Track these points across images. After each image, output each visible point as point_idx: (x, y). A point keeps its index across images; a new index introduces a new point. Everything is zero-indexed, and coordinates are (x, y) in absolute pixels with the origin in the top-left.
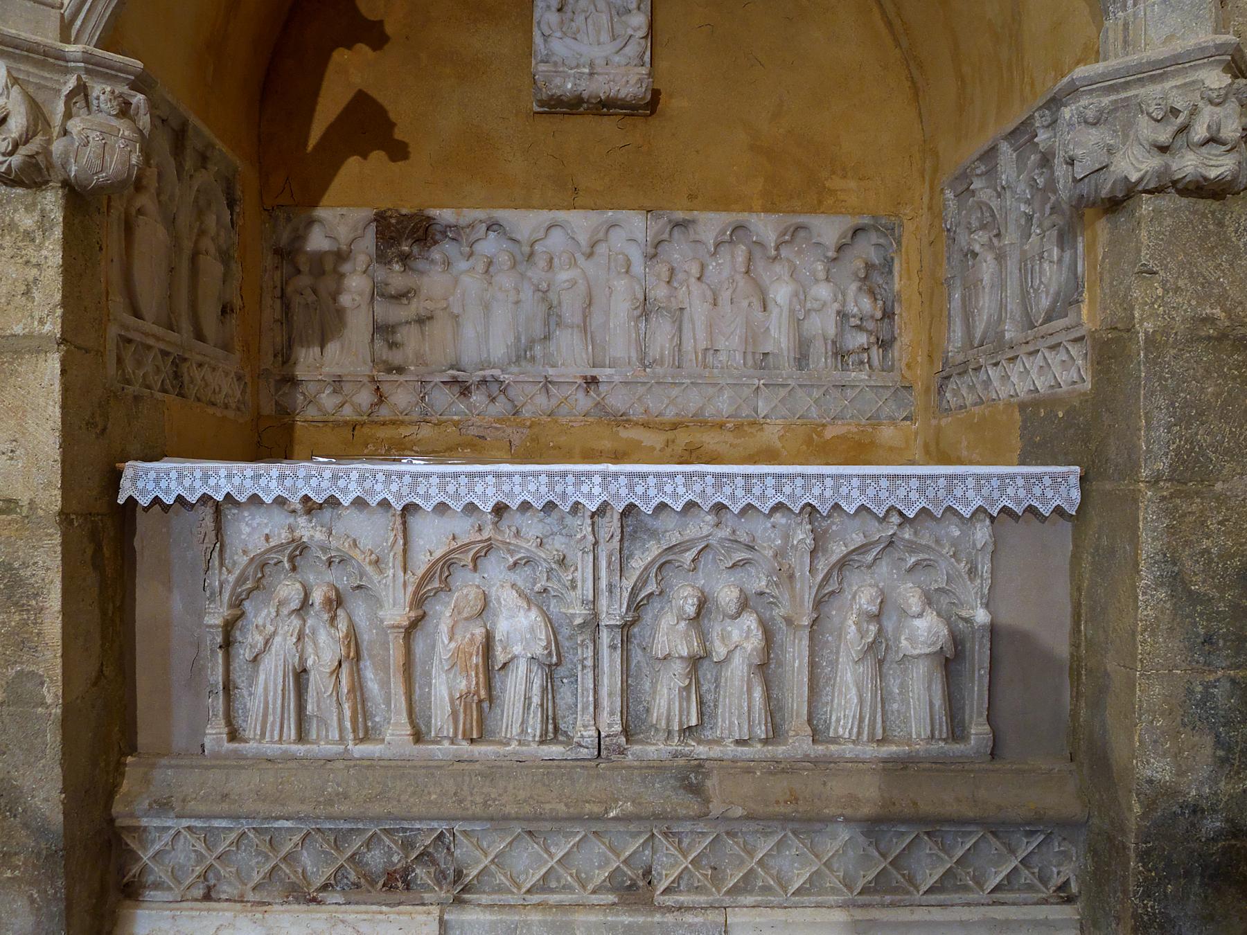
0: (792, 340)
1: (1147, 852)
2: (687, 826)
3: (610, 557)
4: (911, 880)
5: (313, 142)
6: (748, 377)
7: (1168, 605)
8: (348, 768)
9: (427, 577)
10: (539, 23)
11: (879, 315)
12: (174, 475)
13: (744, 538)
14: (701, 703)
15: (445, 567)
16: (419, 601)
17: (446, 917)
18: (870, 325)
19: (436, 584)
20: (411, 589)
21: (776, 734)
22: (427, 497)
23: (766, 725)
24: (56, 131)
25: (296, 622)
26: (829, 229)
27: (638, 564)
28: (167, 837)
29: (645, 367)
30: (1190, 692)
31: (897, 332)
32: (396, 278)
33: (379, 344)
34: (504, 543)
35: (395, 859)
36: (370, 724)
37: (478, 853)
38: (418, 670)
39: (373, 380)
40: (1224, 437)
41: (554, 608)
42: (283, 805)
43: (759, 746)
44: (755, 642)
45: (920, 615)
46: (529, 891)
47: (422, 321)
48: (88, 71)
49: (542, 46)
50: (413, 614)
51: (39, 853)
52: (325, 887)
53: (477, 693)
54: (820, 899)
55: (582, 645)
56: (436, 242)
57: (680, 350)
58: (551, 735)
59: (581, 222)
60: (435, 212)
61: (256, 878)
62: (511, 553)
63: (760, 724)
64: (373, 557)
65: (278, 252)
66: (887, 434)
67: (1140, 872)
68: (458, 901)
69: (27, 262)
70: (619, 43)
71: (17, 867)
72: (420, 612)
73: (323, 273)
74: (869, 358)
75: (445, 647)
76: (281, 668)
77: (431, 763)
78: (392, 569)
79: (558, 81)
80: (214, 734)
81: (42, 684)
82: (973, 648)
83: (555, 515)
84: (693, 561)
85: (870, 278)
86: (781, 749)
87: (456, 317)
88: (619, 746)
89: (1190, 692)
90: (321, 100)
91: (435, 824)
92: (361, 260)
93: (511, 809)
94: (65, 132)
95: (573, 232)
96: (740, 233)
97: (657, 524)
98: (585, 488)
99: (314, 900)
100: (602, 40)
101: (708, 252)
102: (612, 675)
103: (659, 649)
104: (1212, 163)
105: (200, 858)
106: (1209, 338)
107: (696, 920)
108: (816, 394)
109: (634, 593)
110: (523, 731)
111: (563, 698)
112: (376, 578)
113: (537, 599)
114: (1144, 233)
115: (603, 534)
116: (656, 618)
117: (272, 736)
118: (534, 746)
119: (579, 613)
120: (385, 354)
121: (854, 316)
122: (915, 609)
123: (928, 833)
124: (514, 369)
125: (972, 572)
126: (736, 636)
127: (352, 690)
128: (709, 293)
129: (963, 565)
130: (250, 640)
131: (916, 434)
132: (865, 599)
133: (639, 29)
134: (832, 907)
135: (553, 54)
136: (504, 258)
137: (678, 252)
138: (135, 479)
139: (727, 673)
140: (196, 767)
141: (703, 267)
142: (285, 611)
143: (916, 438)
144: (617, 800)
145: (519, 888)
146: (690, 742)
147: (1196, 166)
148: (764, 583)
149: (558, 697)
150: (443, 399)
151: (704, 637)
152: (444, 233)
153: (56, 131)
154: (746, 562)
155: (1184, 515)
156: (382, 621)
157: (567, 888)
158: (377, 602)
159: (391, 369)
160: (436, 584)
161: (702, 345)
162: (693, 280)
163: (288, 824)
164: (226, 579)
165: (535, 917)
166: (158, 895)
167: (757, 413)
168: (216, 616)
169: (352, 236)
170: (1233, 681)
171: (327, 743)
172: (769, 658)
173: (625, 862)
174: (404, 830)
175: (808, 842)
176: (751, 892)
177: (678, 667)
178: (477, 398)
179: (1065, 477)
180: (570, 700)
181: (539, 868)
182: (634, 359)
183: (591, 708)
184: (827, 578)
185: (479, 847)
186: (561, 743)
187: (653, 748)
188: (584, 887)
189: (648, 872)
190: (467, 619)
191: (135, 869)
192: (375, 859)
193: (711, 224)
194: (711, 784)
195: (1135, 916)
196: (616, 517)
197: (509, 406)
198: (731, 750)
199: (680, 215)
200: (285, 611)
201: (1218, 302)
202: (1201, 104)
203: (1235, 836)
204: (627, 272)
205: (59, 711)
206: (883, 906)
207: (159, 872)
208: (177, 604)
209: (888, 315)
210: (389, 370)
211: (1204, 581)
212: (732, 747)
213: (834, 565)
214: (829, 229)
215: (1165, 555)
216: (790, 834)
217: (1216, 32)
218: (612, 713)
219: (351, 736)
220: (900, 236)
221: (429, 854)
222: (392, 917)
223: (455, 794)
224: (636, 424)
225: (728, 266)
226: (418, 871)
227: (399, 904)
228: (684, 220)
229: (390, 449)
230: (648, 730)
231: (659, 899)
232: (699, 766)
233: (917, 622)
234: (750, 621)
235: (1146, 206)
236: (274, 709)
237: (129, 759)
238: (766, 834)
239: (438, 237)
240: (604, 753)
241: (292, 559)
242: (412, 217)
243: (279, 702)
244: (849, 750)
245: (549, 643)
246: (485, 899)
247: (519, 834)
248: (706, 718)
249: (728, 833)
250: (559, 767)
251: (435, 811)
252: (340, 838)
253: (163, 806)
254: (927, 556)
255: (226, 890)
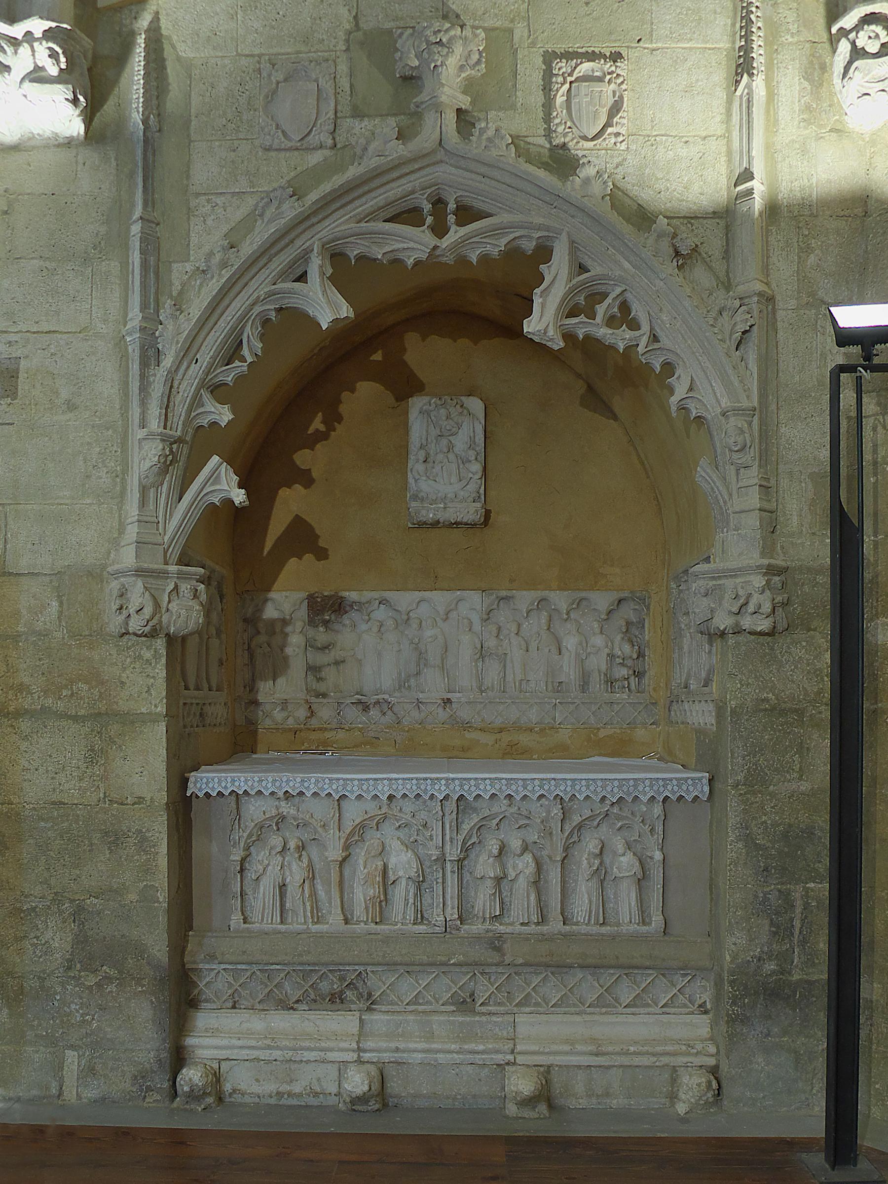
0: (577, 673)
1: (734, 981)
2: (493, 969)
3: (451, 823)
4: (617, 1000)
5: (265, 552)
6: (549, 698)
7: (744, 851)
8: (310, 937)
9: (352, 834)
10: (411, 470)
11: (635, 656)
12: (216, 780)
13: (525, 813)
14: (502, 903)
15: (361, 828)
16: (347, 847)
17: (363, 1017)
18: (629, 663)
19: (356, 838)
20: (342, 841)
21: (543, 920)
22: (352, 792)
23: (537, 915)
24: (164, 610)
25: (280, 858)
26: (602, 600)
27: (466, 827)
28: (213, 974)
29: (482, 692)
30: (756, 897)
31: (647, 667)
32: (321, 636)
33: (310, 677)
34: (393, 815)
35: (335, 987)
36: (320, 914)
37: (380, 983)
38: (346, 885)
39: (307, 701)
40: (774, 762)
41: (421, 851)
42: (276, 957)
43: (534, 926)
44: (531, 868)
45: (624, 855)
46: (407, 1004)
47: (337, 663)
48: (178, 578)
49: (414, 485)
50: (344, 854)
51: (156, 978)
52: (297, 1001)
53: (379, 897)
54: (566, 1009)
55: (436, 870)
56: (346, 612)
57: (504, 680)
58: (420, 920)
59: (440, 599)
60: (345, 594)
61: (261, 997)
62: (398, 821)
63: (534, 914)
64: (322, 823)
65: (246, 620)
66: (640, 734)
67: (730, 992)
68: (369, 1009)
69: (148, 675)
70: (464, 483)
71: (144, 985)
72: (348, 853)
73: (274, 633)
74: (629, 683)
75: (361, 872)
76: (272, 884)
77: (354, 935)
78: (333, 831)
79: (424, 512)
80: (236, 919)
81: (158, 891)
82: (654, 873)
83: (421, 800)
84: (497, 825)
85: (631, 630)
86: (546, 928)
87: (359, 661)
88: (457, 926)
89: (756, 897)
90: (271, 522)
91: (357, 967)
92: (299, 625)
93: (398, 959)
94: (168, 610)
95: (435, 605)
96: (543, 603)
97: (477, 805)
98: (437, 787)
99: (292, 1008)
100: (452, 481)
101: (523, 616)
102: (452, 887)
103: (479, 871)
104: (759, 623)
105: (230, 985)
106: (766, 710)
107: (498, 1019)
108: (594, 708)
109: (464, 842)
110: (405, 918)
111: (426, 900)
112: (324, 834)
113: (411, 845)
114: (730, 655)
115: (447, 811)
116: (477, 856)
117: (267, 920)
118: (410, 925)
119: (435, 853)
120: (315, 685)
121: (618, 657)
122: (621, 851)
123: (626, 974)
124: (397, 694)
125: (652, 830)
126: (521, 866)
127: (310, 896)
128: (523, 643)
129: (647, 827)
130: (254, 869)
131: (660, 733)
132: (591, 844)
133: (476, 473)
134: (573, 1014)
135: (421, 491)
136: (390, 623)
137: (503, 616)
138: (195, 783)
139: (516, 886)
140: (227, 937)
141: (519, 626)
142: (274, 853)
143: (659, 736)
144: (455, 955)
145: (402, 1003)
146: (496, 924)
147: (750, 625)
148: (536, 837)
149: (423, 899)
150: (352, 714)
151: (503, 867)
152: (351, 606)
153: (164, 610)
154: (527, 825)
155: (752, 803)
156: (327, 858)
157: (428, 1003)
158: (325, 848)
159: (318, 695)
160: (356, 838)
161: (518, 678)
162: (513, 634)
163: (278, 967)
164: (241, 835)
165: (411, 1017)
166: (209, 1005)
167: (555, 722)
168: (236, 855)
169: (292, 610)
170: (779, 891)
171: (297, 924)
172: (539, 878)
173: (459, 988)
174: (340, 970)
175: (560, 979)
176: (529, 1006)
177: (489, 883)
178: (374, 712)
179: (700, 779)
180: (430, 901)
181: (413, 991)
182: (474, 687)
183: (442, 905)
184: (571, 834)
185: (380, 980)
186: (425, 924)
187: (475, 927)
188: (438, 1002)
189: (472, 995)
190: (373, 857)
191: (196, 992)
192: (324, 986)
193: (525, 598)
194: (507, 946)
195: (728, 1015)
196: (454, 802)
197: (394, 718)
198: (518, 928)
199: (504, 593)
200: (274, 853)
201: (771, 691)
202: (753, 592)
203: (782, 974)
204: (470, 630)
205: (166, 905)
206: (601, 1014)
207: (209, 993)
208: (215, 848)
209: (641, 655)
210: (317, 696)
211: (763, 838)
212: (519, 927)
213: (575, 827)
214: (602, 600)
215: (742, 825)
216: (550, 974)
217: (763, 555)
218: (453, 908)
219: (311, 920)
220: (649, 604)
221: (354, 984)
222: (334, 1017)
223: (368, 951)
224: (476, 729)
225: (535, 624)
226: (347, 993)
227: (338, 1011)
228: (507, 596)
229: (318, 746)
230: (473, 918)
231: (478, 1008)
232: (500, 937)
233: (622, 859)
234: (528, 858)
235: (731, 640)
236: (268, 906)
237: (191, 933)
238: (536, 974)
239: (348, 608)
240: (448, 930)
241: (277, 824)
242: (329, 597)
243: (271, 902)
244: (583, 929)
245: (418, 870)
246: (384, 1008)
247: (402, 973)
248: (505, 911)
249: (515, 973)
250: (424, 937)
251: (357, 960)
252: (306, 975)
253: (212, 957)
254: (627, 822)
255: (244, 1003)
